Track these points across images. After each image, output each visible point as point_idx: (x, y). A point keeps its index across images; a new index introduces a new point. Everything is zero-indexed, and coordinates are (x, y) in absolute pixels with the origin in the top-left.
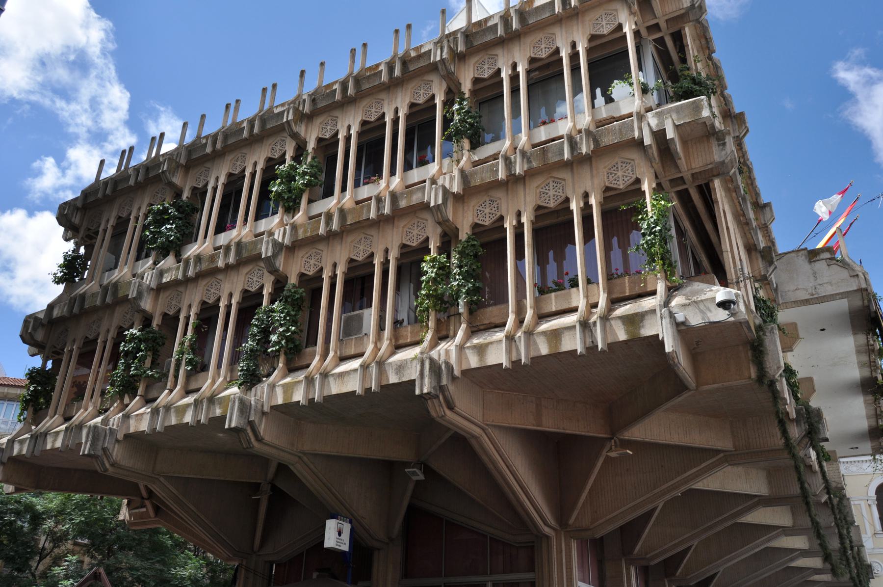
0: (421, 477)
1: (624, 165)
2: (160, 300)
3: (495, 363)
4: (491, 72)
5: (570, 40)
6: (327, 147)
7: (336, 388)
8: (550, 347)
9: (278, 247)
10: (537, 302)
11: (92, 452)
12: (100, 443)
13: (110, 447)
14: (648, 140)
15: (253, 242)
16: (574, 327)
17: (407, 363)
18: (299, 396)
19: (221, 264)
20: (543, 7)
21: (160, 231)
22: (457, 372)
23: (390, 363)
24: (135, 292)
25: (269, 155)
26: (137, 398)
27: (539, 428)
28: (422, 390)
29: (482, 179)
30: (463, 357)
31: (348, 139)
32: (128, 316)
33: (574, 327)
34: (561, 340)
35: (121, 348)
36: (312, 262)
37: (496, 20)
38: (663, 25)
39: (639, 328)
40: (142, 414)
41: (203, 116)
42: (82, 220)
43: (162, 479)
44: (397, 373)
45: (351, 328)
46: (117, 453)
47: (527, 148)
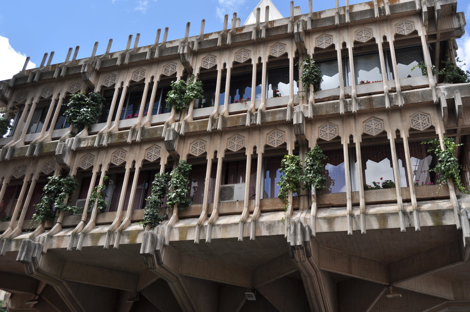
0: (254, 299)
1: (423, 117)
2: (76, 159)
3: (340, 231)
4: (328, 45)
5: (382, 35)
6: (107, 93)
7: (220, 234)
8: (380, 224)
9: (177, 135)
10: (133, 213)
11: (26, 260)
12: (31, 254)
13: (38, 257)
14: (444, 104)
15: (22, 148)
16: (397, 213)
17: (281, 222)
18: (193, 236)
19: (129, 140)
20: (405, 4)
21: (79, 112)
22: (314, 234)
23: (262, 222)
24: (61, 151)
25: (163, 73)
26: (57, 224)
27: (350, 275)
28: (144, 251)
29: (327, 112)
30: (317, 224)
31: (121, 90)
32: (49, 167)
33: (397, 213)
34: (387, 220)
35: (46, 188)
36: (198, 148)
37: (147, 50)
38: (439, 36)
39: (442, 219)
40: (63, 236)
41: (111, 40)
42: (11, 96)
43: (64, 283)
44: (267, 229)
45: (225, 195)
46: (41, 262)
47: (227, 115)
